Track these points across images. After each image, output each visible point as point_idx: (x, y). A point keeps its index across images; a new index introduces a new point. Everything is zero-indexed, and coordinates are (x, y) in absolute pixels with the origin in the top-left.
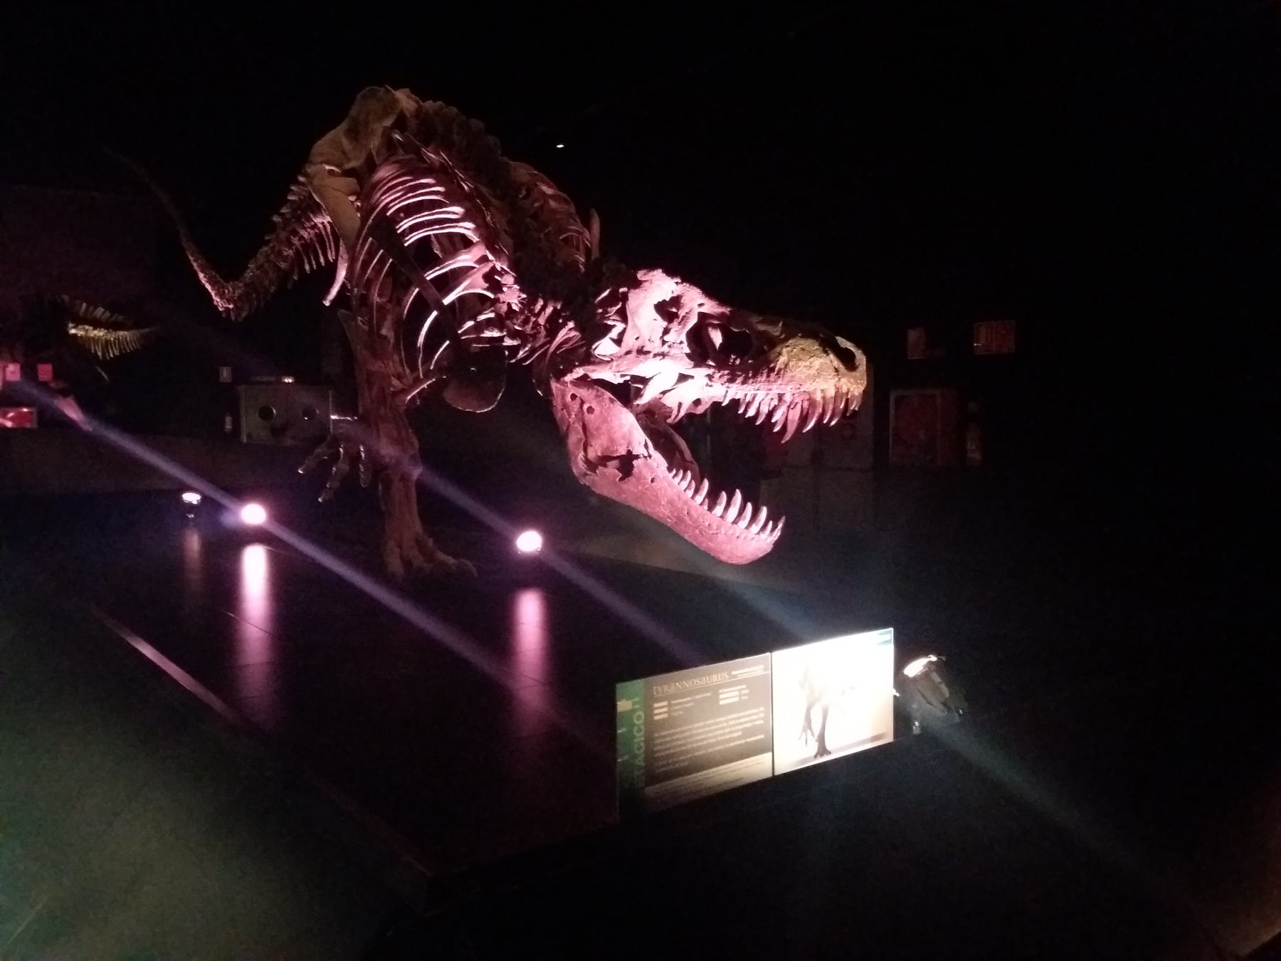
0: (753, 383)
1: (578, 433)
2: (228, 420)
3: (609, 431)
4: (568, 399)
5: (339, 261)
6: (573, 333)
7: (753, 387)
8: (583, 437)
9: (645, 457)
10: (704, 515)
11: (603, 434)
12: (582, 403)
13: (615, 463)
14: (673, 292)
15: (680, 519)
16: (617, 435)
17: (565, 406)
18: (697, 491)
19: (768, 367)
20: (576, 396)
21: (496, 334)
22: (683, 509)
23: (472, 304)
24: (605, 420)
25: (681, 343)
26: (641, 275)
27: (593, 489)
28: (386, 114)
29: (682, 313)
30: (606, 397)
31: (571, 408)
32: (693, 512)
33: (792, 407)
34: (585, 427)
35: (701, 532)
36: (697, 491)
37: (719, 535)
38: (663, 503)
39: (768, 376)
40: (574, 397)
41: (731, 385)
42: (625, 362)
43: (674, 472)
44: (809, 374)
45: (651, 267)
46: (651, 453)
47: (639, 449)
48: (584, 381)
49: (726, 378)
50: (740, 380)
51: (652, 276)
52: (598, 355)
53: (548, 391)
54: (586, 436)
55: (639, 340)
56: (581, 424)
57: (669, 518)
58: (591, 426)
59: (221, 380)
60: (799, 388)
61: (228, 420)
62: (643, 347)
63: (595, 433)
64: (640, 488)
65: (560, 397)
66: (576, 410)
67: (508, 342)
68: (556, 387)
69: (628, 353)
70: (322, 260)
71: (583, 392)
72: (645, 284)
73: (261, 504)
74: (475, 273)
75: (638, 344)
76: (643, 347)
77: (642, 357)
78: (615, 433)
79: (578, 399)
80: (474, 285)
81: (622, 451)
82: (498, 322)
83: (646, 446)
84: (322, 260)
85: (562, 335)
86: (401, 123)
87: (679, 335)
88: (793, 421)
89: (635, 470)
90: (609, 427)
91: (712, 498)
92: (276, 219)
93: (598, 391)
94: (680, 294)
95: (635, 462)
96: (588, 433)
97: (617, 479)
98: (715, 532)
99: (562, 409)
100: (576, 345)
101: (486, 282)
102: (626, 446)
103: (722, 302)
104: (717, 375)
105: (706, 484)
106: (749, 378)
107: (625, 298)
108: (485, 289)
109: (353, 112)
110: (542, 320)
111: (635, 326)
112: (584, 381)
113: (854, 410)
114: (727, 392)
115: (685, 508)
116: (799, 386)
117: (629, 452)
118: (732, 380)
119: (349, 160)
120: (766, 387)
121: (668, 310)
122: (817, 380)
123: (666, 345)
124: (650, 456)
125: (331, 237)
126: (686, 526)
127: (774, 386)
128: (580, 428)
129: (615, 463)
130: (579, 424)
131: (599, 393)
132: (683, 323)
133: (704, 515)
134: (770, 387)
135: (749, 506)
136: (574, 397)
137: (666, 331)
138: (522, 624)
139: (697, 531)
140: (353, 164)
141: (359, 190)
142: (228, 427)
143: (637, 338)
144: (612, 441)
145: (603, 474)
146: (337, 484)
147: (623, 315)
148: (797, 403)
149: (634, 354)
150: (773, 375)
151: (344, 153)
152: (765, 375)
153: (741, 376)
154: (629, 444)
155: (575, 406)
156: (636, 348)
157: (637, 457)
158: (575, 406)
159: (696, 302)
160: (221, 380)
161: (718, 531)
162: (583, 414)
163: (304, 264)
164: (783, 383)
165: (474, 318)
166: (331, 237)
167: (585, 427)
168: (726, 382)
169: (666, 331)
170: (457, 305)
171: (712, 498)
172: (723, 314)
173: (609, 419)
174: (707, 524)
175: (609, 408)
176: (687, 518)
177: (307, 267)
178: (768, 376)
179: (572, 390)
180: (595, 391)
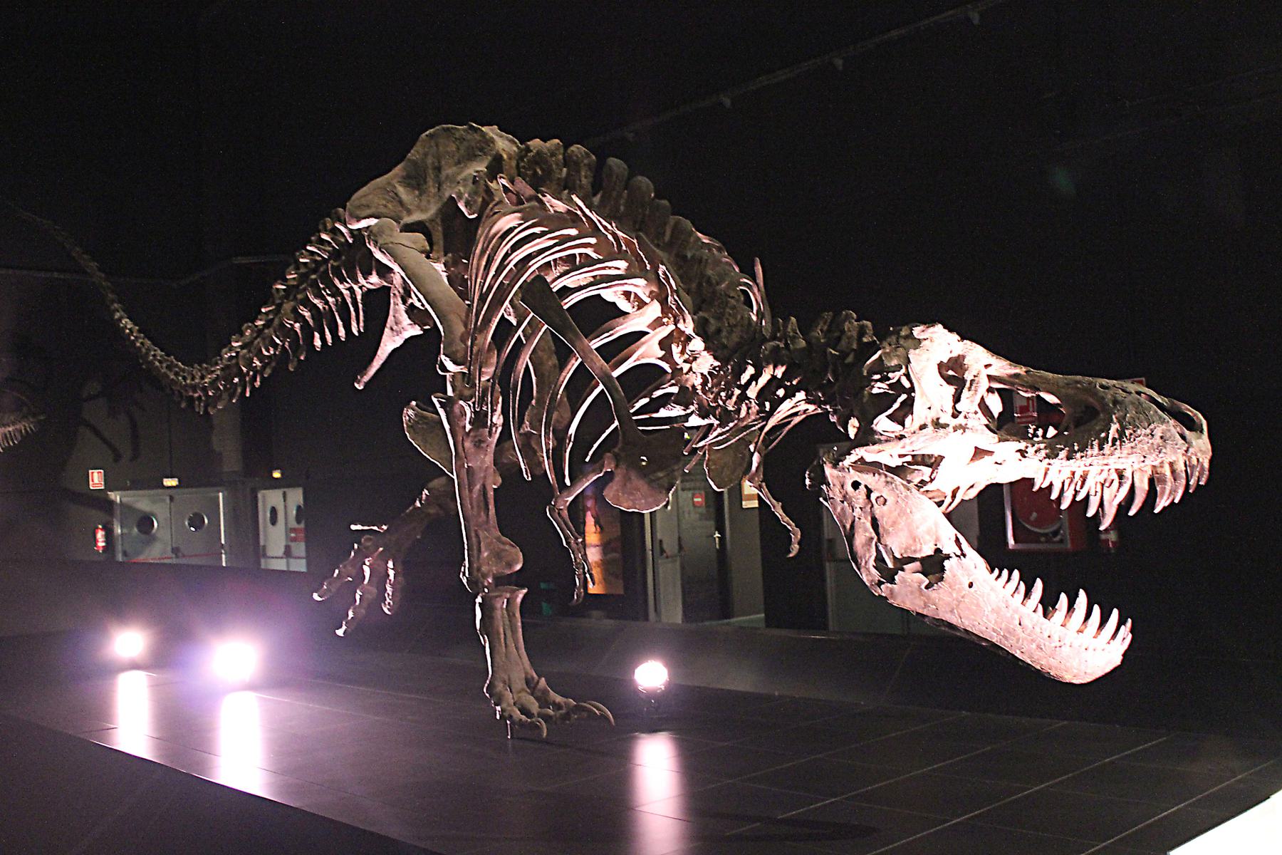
0: (1082, 457)
1: (866, 530)
3: (909, 525)
4: (849, 488)
5: (384, 337)
6: (803, 406)
7: (1083, 463)
8: (874, 535)
9: (957, 556)
10: (1042, 624)
11: (902, 530)
12: (869, 491)
13: (917, 565)
16: (921, 531)
17: (845, 498)
18: (1028, 594)
19: (1098, 437)
20: (860, 484)
21: (677, 411)
22: (1013, 618)
23: (647, 376)
24: (903, 513)
25: (976, 413)
26: (917, 331)
27: (891, 601)
28: (471, 157)
29: (968, 376)
33: (1107, 484)
34: (875, 524)
36: (1028, 594)
37: (1063, 648)
38: (986, 613)
39: (1101, 448)
40: (856, 485)
41: (1051, 461)
42: (922, 439)
43: (997, 571)
44: (1152, 444)
45: (930, 322)
47: (949, 548)
48: (862, 465)
49: (1043, 453)
50: (1063, 454)
51: (932, 333)
53: (821, 479)
54: (877, 534)
58: (883, 522)
60: (1143, 462)
62: (938, 419)
63: (891, 529)
64: (954, 595)
65: (839, 487)
67: (695, 421)
68: (831, 475)
69: (923, 427)
70: (342, 332)
71: (866, 479)
72: (924, 343)
74: (650, 339)
75: (933, 415)
76: (938, 419)
78: (917, 528)
79: (862, 487)
80: (649, 352)
81: (928, 551)
82: (685, 397)
84: (342, 332)
85: (785, 408)
86: (496, 167)
89: (947, 574)
90: (909, 521)
91: (1048, 604)
93: (886, 476)
94: (961, 353)
95: (946, 563)
96: (881, 530)
97: (923, 587)
98: (1058, 644)
99: (842, 502)
100: (783, 422)
101: (662, 349)
102: (933, 543)
103: (1014, 359)
104: (1031, 450)
105: (1039, 584)
106: (1076, 452)
108: (659, 359)
109: (413, 155)
110: (752, 392)
112: (862, 465)
113: (809, 485)
114: (1048, 469)
115: (1017, 617)
116: (1143, 459)
117: (938, 551)
118: (1052, 455)
119: (409, 212)
120: (1102, 462)
121: (953, 372)
122: (1164, 450)
123: (961, 416)
124: (964, 555)
125: (360, 306)
127: (1111, 460)
128: (869, 525)
129: (917, 565)
130: (866, 518)
131: (889, 479)
132: (973, 388)
134: (1105, 462)
135: (1096, 609)
136: (856, 485)
137: (957, 399)
138: (678, 772)
140: (416, 217)
141: (428, 248)
145: (903, 581)
148: (1113, 480)
149: (930, 428)
150: (1107, 447)
151: (401, 203)
152: (1096, 448)
153: (1063, 449)
154: (937, 539)
155: (860, 496)
157: (948, 557)
159: (979, 359)
161: (1062, 643)
164: (1123, 456)
165: (649, 395)
166: (360, 306)
167: (875, 524)
168: (1045, 458)
169: (957, 399)
171: (1048, 604)
172: (1017, 376)
173: (908, 511)
174: (1046, 635)
177: (318, 343)
178: (1101, 448)
179: (854, 476)
180: (883, 476)
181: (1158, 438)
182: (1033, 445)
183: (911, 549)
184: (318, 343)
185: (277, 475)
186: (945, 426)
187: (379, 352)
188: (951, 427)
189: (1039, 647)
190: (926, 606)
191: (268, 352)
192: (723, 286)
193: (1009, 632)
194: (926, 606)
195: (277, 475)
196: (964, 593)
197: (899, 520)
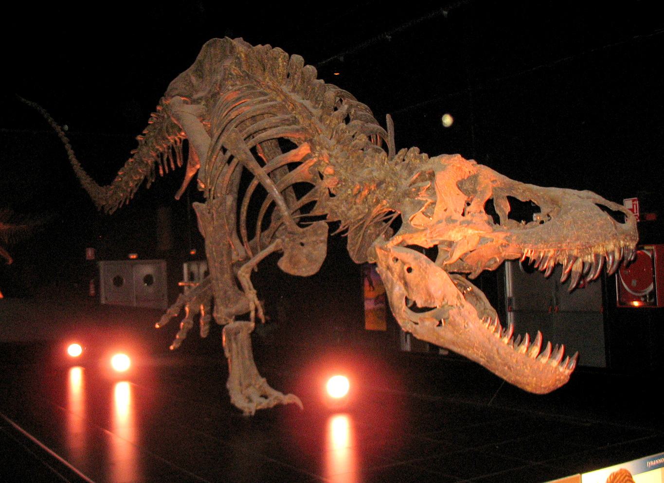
2: (92, 287)
10: (512, 353)
14: (470, 172)
15: (490, 358)
17: (388, 268)
30: (422, 258)
31: (394, 269)
32: (501, 352)
35: (509, 368)
46: (463, 303)
52: (415, 225)
55: (448, 211)
56: (403, 282)
57: (482, 357)
59: (87, 258)
61: (92, 287)
66: (398, 270)
70: (173, 166)
73: (80, 355)
77: (451, 225)
79: (399, 261)
83: (458, 297)
84: (173, 166)
87: (477, 206)
88: (576, 273)
92: (139, 138)
97: (435, 326)
107: (432, 176)
111: (442, 200)
119: (197, 91)
126: (496, 363)
133: (512, 353)
138: (136, 446)
139: (506, 368)
142: (92, 292)
143: (445, 210)
144: (429, 294)
146: (184, 336)
147: (432, 191)
149: (444, 222)
156: (445, 217)
158: (397, 267)
160: (87, 258)
162: (404, 273)
163: (604, 197)
170: (86, 181)
174: (514, 361)
175: (426, 268)
176: (496, 357)
177: (161, 172)
181: (207, 214)
182: (522, 240)
183: (189, 302)
184: (161, 172)
185: (193, 252)
186: (454, 221)
187: (186, 178)
188: (458, 222)
189: (509, 368)
190: (438, 339)
191: (136, 177)
192: (23, 99)
193: (490, 358)
194: (438, 339)
195: (193, 252)
196: (461, 331)
197: (421, 283)
